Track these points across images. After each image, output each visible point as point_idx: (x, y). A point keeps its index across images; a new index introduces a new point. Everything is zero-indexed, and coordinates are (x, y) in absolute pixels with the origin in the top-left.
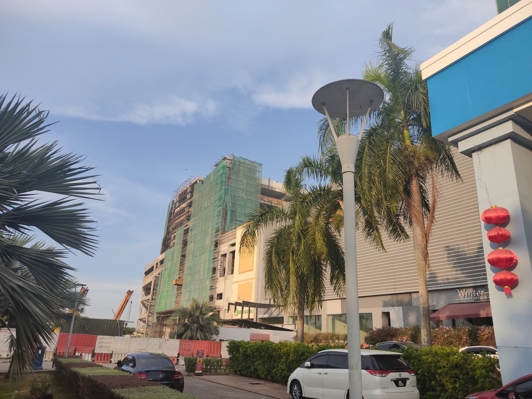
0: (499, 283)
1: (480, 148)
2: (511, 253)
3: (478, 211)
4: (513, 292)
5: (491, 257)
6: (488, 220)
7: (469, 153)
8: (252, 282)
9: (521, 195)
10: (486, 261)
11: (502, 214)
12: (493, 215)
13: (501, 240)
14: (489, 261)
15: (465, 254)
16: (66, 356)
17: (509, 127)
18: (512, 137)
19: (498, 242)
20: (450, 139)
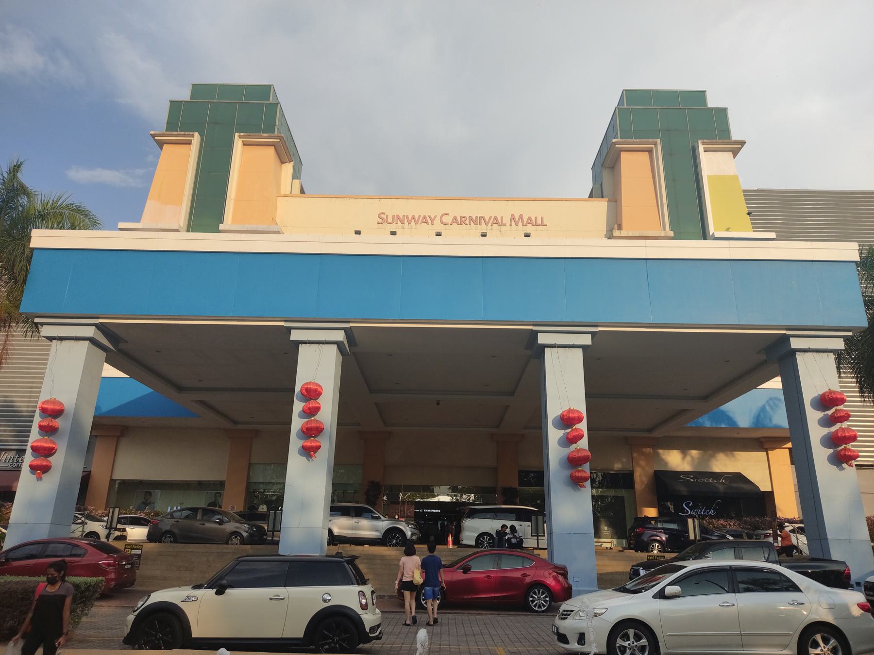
0: (33, 468)
1: (61, 339)
2: (54, 443)
3: (38, 397)
4: (44, 476)
5: (35, 444)
6: (44, 410)
7: (51, 339)
8: (234, 222)
9: (80, 394)
10: (29, 444)
11: (57, 407)
12: (49, 407)
13: (48, 430)
14: (32, 448)
15: (20, 411)
16: (390, 220)
17: (90, 332)
18: (92, 340)
19: (47, 432)
20: (36, 320)
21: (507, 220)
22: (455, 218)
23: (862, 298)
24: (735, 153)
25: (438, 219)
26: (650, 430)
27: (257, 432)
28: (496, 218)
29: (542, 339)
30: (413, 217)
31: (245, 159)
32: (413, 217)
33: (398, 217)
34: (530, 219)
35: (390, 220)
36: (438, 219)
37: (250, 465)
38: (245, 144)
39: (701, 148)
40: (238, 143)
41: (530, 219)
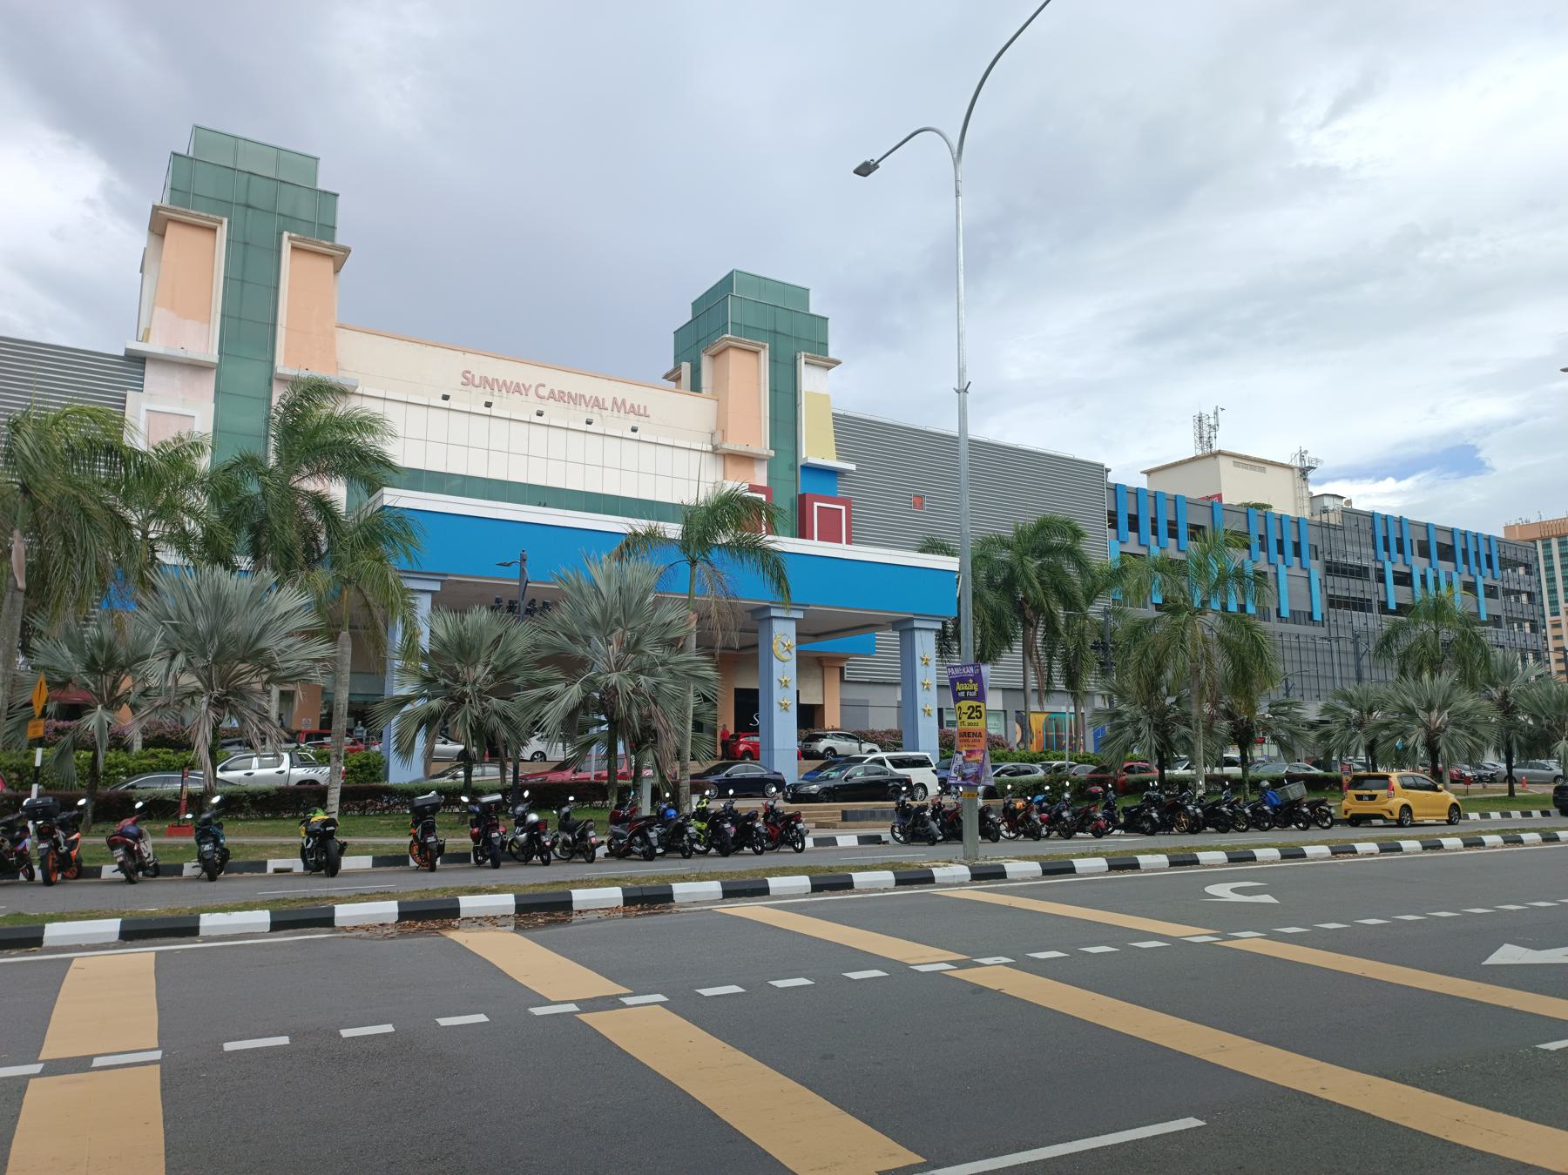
16: (477, 382)
21: (609, 404)
22: (552, 392)
25: (532, 392)
34: (632, 406)
35: (477, 382)
38: (294, 248)
41: (632, 406)
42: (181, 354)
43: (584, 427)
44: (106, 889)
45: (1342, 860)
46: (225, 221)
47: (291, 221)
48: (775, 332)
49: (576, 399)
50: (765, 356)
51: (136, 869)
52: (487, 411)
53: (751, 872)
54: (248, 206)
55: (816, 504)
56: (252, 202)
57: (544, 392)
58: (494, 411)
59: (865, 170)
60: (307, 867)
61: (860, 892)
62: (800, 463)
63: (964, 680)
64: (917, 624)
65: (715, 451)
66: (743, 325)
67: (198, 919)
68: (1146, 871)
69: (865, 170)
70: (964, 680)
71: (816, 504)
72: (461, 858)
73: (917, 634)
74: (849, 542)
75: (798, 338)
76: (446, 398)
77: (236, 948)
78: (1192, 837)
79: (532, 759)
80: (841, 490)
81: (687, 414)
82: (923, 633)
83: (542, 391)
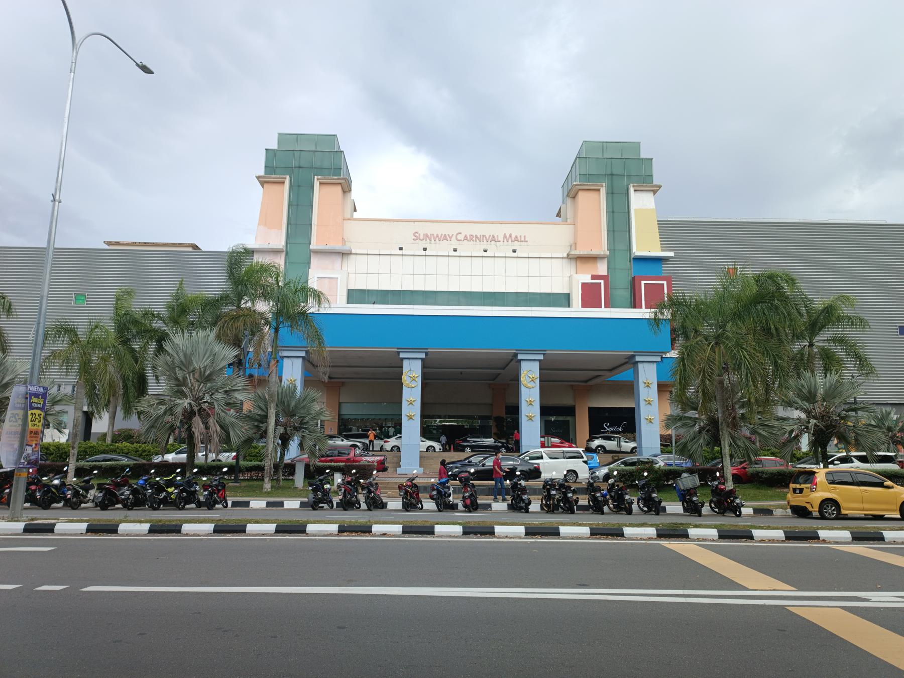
16: (422, 237)
21: (501, 238)
22: (466, 236)
23: (402, 435)
24: (655, 192)
25: (454, 238)
26: (586, 381)
27: (343, 383)
28: (493, 236)
29: (520, 357)
30: (437, 236)
31: (322, 197)
32: (437, 236)
33: (427, 236)
34: (516, 237)
35: (422, 237)
36: (454, 238)
37: (340, 403)
38: (321, 183)
39: (632, 190)
40: (317, 184)
41: (516, 237)
42: (271, 246)
43: (482, 254)
44: (362, 513)
45: (861, 549)
46: (288, 177)
47: (320, 170)
48: (612, 175)
49: (479, 238)
50: (603, 191)
51: (472, 506)
52: (400, 252)
53: (745, 526)
54: (300, 167)
55: (643, 283)
56: (302, 165)
57: (460, 237)
58: (428, 253)
59: (146, 69)
60: (685, 509)
61: (250, 535)
62: (632, 256)
63: (37, 396)
64: (638, 359)
65: (569, 257)
66: (613, 172)
67: (306, 526)
68: (890, 543)
69: (146, 69)
70: (37, 396)
71: (643, 283)
72: (583, 508)
73: (640, 366)
74: (606, 306)
75: (629, 176)
76: (401, 249)
77: (197, 543)
78: (549, 515)
79: (392, 450)
80: (666, 270)
81: (558, 237)
82: (646, 365)
83: (459, 237)
